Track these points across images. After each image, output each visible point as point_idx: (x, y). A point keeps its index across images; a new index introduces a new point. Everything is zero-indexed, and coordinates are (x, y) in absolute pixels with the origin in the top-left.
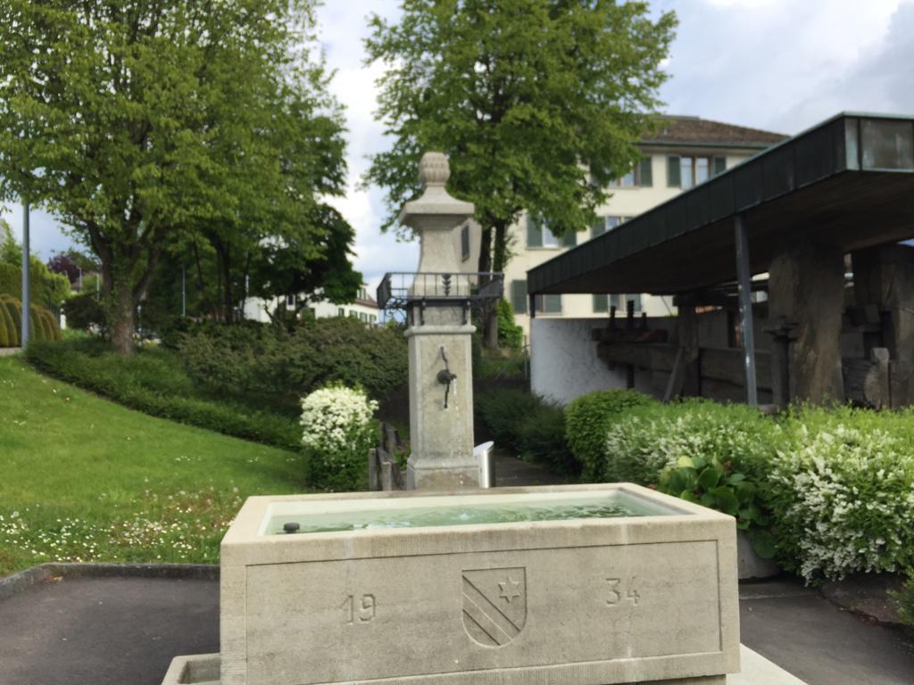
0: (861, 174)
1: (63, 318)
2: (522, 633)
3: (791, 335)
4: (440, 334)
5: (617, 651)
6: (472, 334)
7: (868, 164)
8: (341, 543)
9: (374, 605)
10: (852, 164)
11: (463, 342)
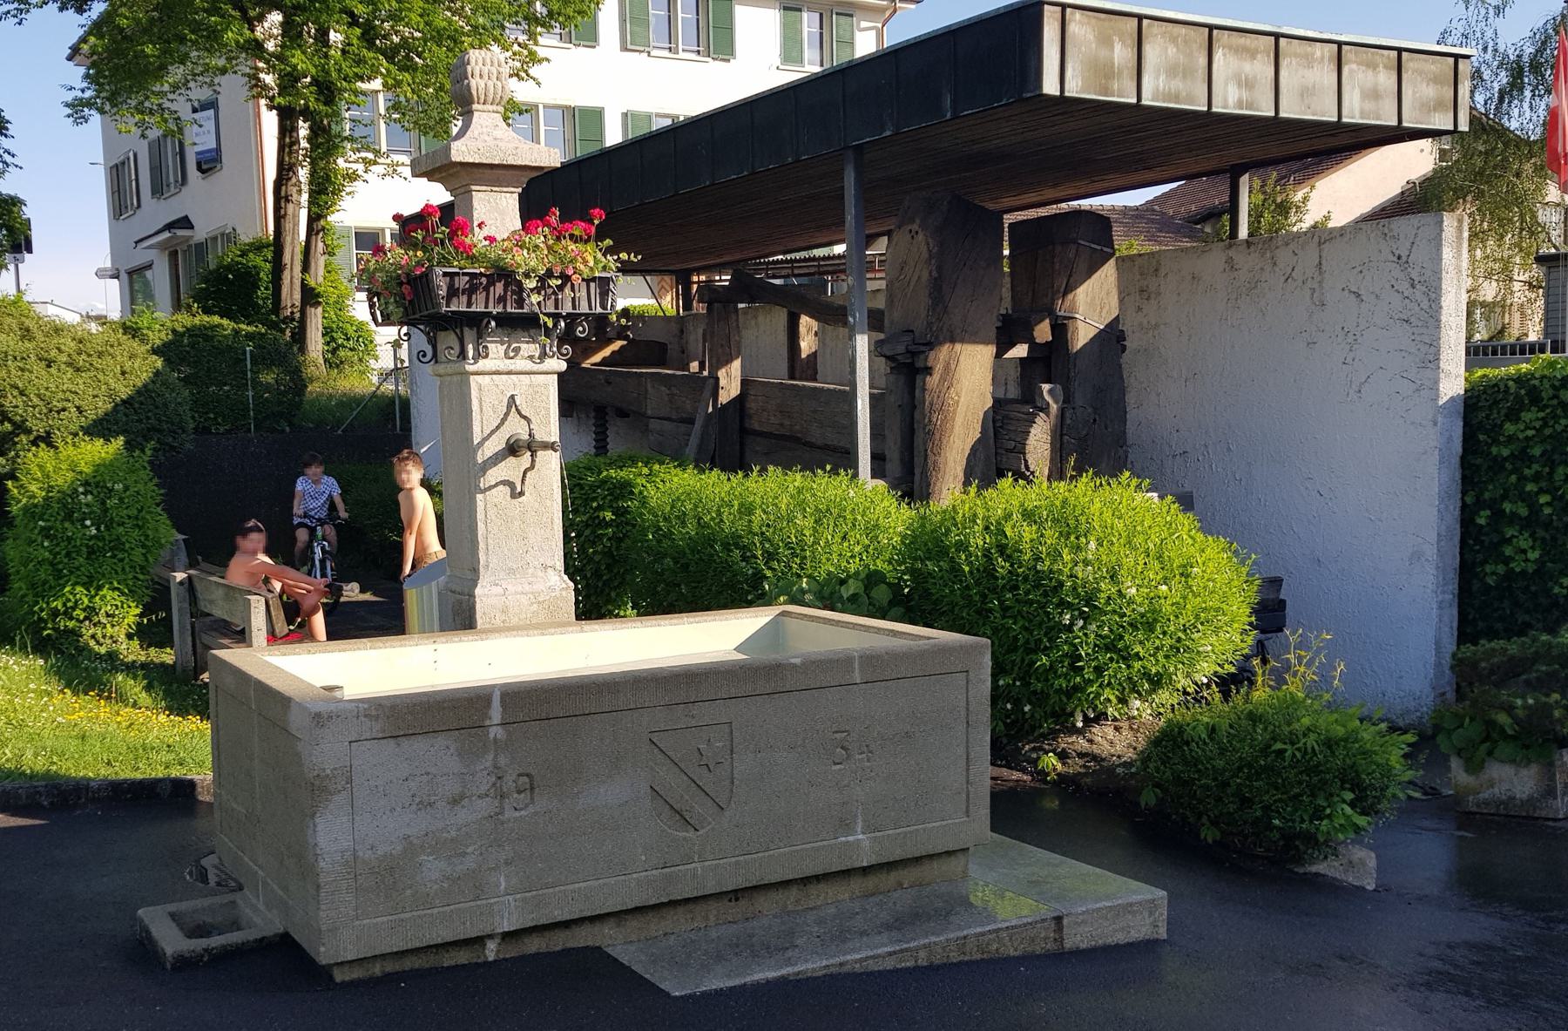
0: (1062, 100)
1: (862, 343)
2: (727, 813)
3: (920, 364)
4: (509, 373)
5: (846, 826)
6: (561, 375)
7: (1073, 90)
8: (891, 942)
9: (532, 789)
10: (1050, 87)
11: (546, 386)
